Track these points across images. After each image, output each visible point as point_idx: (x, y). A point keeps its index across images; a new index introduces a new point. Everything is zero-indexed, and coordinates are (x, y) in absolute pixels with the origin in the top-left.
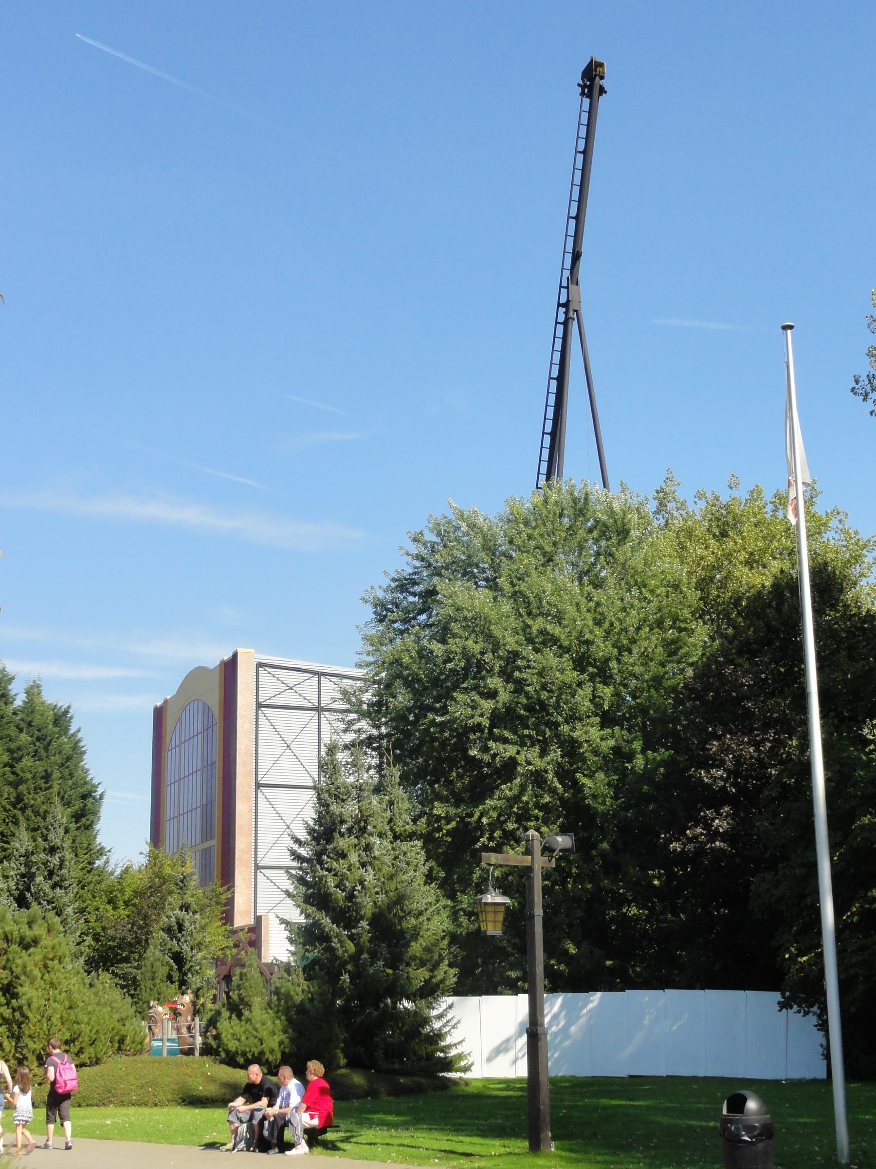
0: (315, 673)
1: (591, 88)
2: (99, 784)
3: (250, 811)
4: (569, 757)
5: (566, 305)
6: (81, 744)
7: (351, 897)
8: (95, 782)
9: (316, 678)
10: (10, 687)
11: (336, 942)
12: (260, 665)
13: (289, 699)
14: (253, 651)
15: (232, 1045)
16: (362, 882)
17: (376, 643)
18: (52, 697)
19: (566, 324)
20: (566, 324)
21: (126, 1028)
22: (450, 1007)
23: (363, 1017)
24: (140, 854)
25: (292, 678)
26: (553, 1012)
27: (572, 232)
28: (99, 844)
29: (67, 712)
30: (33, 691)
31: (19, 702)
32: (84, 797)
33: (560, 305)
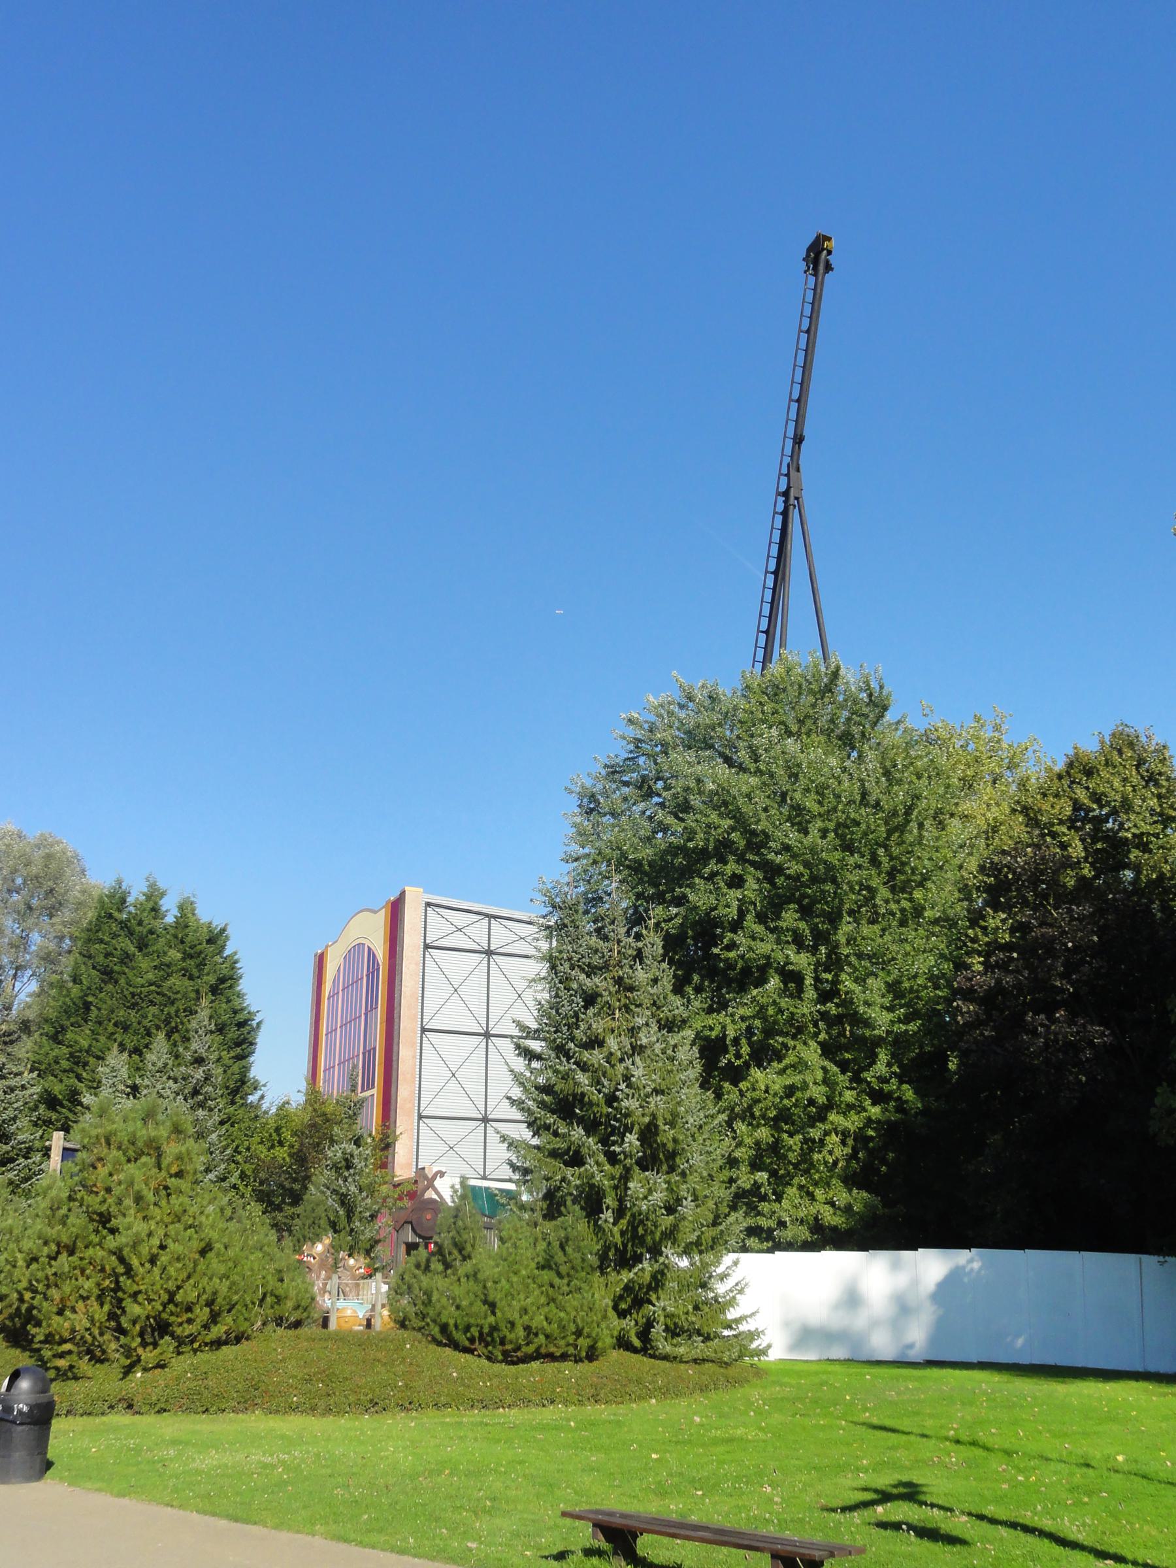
1: (816, 262)
2: (258, 1012)
3: (414, 1057)
4: (323, 1269)
5: (786, 494)
6: (238, 965)
7: (611, 1099)
10: (161, 902)
11: (592, 1163)
12: (428, 905)
13: (458, 941)
14: (422, 890)
15: (450, 1315)
16: (627, 1078)
17: (583, 836)
18: (208, 914)
19: (785, 514)
20: (785, 514)
22: (736, 1263)
23: (631, 1275)
24: (299, 1091)
25: (460, 919)
27: (793, 416)
28: (254, 1078)
29: (223, 930)
30: (186, 908)
31: (170, 919)
32: (241, 1025)
33: (778, 494)
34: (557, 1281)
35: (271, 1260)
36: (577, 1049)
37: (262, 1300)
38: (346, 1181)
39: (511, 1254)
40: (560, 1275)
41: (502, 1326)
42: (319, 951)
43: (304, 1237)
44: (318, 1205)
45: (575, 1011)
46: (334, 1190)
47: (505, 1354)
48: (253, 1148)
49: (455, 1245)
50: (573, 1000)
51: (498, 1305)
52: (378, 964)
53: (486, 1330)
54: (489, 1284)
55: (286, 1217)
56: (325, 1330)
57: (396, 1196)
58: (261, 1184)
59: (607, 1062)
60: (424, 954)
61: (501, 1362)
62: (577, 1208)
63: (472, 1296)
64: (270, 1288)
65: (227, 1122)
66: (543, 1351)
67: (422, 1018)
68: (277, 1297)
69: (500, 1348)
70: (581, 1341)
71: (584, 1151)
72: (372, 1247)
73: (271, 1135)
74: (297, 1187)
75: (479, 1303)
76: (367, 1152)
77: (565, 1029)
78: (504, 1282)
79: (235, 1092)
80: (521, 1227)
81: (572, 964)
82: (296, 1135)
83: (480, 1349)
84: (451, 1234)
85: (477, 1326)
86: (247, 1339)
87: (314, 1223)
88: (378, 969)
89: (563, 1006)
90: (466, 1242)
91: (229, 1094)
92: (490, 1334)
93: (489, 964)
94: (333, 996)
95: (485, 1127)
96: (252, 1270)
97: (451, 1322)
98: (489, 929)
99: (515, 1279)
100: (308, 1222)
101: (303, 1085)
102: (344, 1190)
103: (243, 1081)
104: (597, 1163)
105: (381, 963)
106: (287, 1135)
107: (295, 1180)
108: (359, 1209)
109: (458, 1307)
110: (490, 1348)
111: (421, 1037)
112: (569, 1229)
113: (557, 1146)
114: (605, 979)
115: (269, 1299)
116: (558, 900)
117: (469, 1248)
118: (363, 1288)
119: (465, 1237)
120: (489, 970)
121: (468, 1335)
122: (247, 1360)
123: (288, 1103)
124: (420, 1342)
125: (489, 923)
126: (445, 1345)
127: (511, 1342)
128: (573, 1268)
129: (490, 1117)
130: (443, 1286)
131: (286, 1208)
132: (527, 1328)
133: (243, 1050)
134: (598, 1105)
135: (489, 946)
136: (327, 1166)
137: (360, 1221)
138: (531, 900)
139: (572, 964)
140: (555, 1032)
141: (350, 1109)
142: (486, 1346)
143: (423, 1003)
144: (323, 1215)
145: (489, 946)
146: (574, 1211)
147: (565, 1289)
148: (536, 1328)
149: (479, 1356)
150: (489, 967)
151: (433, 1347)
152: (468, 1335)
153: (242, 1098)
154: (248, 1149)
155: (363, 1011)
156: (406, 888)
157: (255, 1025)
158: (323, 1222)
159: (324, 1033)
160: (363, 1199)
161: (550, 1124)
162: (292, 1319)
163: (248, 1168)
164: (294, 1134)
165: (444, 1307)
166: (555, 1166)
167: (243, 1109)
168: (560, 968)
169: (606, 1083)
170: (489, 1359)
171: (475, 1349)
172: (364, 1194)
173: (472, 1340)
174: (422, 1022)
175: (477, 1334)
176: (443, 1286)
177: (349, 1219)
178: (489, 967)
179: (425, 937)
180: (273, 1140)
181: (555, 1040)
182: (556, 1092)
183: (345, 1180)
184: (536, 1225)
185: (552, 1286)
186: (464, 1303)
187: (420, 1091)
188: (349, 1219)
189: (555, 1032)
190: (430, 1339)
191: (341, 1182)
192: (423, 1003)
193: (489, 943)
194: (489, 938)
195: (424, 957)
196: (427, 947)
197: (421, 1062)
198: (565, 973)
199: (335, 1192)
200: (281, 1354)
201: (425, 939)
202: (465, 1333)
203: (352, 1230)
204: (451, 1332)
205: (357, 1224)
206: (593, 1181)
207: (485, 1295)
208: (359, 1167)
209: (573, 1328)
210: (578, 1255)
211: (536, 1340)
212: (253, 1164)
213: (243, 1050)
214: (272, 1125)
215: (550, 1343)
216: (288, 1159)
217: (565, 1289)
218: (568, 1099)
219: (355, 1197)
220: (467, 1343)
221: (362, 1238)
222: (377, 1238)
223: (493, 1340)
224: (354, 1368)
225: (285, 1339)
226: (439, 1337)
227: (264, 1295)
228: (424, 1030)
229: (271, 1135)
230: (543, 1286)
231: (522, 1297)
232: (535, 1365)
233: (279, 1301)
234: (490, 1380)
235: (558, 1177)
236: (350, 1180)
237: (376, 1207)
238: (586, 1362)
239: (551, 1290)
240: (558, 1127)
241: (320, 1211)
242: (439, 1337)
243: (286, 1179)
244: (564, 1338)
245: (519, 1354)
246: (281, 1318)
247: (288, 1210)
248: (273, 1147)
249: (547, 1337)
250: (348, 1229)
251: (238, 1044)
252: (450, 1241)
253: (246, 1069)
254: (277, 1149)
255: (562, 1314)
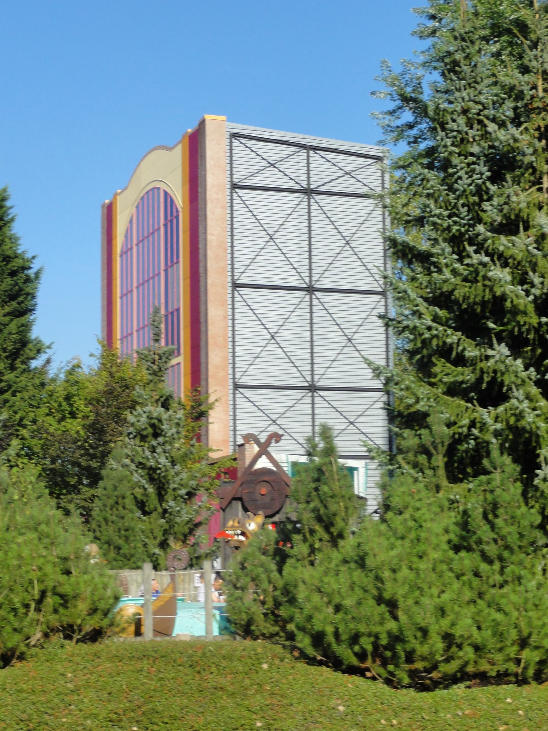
0: (303, 146)
2: (33, 258)
3: (225, 317)
8: (28, 255)
9: (304, 153)
11: (522, 398)
12: (234, 136)
14: (224, 118)
21: (73, 579)
24: (91, 355)
26: (457, 378)
28: (35, 339)
34: (484, 567)
35: (52, 544)
36: (489, 234)
37: (40, 602)
38: (154, 451)
39: (410, 529)
40: (486, 558)
41: (409, 634)
42: (107, 201)
43: (106, 520)
44: (121, 481)
45: (477, 185)
46: (140, 463)
47: (413, 674)
48: (40, 420)
49: (319, 519)
50: (473, 171)
51: (401, 604)
52: (177, 211)
53: (384, 641)
54: (386, 574)
55: (85, 500)
56: (139, 639)
57: (214, 475)
58: (53, 462)
59: (538, 249)
60: (232, 196)
61: (409, 686)
62: (507, 459)
63: (359, 592)
64: (50, 584)
65: (6, 391)
66: (470, 669)
67: (233, 272)
68: (62, 596)
69: (407, 667)
70: (526, 654)
71: (508, 379)
72: (191, 531)
73: (60, 405)
74: (94, 464)
75: (372, 602)
76: (178, 416)
77: (464, 211)
78: (405, 572)
79: (14, 355)
80: (419, 491)
81: (469, 119)
82: (91, 404)
83: (376, 669)
84: (312, 505)
85: (370, 635)
86: (22, 657)
87: (117, 503)
88: (177, 217)
89: (460, 178)
90: (335, 515)
91: (7, 357)
92: (390, 647)
93: (309, 205)
94: (126, 252)
95: (313, 397)
96: (20, 557)
97: (329, 630)
98: (308, 163)
99: (422, 565)
100: (111, 501)
101: (97, 349)
102: (152, 463)
103: (24, 343)
104: (528, 397)
105: (180, 209)
106: (80, 404)
107: (93, 457)
108: (172, 486)
109: (338, 608)
110: (391, 667)
111: (233, 294)
112: (498, 492)
113: (460, 378)
114: (526, 129)
115: (50, 601)
116: (409, 89)
117: (340, 524)
118: (183, 581)
119: (333, 507)
120: (309, 213)
121: (357, 648)
122: (21, 691)
123: (79, 367)
124: (282, 660)
125: (308, 156)
126: (320, 663)
127: (424, 659)
128: (507, 547)
129: (319, 385)
130: (312, 577)
131: (85, 489)
132: (448, 638)
133: (19, 303)
134: (525, 313)
135: (309, 184)
136: (130, 433)
137: (175, 499)
138: (373, 93)
139: (469, 119)
140: (450, 216)
141: (153, 363)
142: (384, 664)
143: (232, 254)
144: (128, 493)
145: (309, 184)
146: (503, 465)
147: (498, 578)
148: (462, 636)
149: (374, 678)
150: (309, 209)
151: (301, 666)
152: (357, 648)
153: (23, 363)
154: (34, 421)
155: (162, 267)
156: (207, 117)
157: (32, 276)
158: (129, 502)
159: (119, 337)
160: (177, 474)
161: (451, 345)
162: (88, 628)
163: (36, 444)
164: (89, 402)
165: (316, 609)
166: (459, 406)
167: (25, 375)
168: (451, 125)
169: (537, 280)
170: (388, 682)
171: (368, 670)
172: (178, 467)
173: (362, 656)
174: (233, 276)
175: (369, 648)
176: (312, 577)
177: (161, 497)
178: (309, 209)
179: (231, 174)
180: (63, 411)
181: (449, 228)
182: (456, 302)
183: (153, 450)
184: (438, 488)
185: (477, 574)
186: (348, 602)
187: (234, 356)
188: (161, 497)
189: (450, 216)
190: (296, 654)
191: (148, 453)
192: (232, 254)
193: (309, 181)
194: (308, 174)
195: (232, 199)
196: (235, 186)
197: (233, 323)
198: (459, 132)
199: (140, 465)
200: (71, 681)
201: (232, 178)
202: (351, 646)
203: (165, 511)
204: (329, 645)
205: (172, 503)
206: (523, 423)
207: (378, 589)
208: (169, 434)
209: (513, 634)
210: (513, 529)
211: (461, 654)
212: (40, 439)
213: (19, 303)
214: (61, 393)
215: (480, 657)
216: (82, 433)
217: (498, 578)
218: (475, 310)
219: (167, 471)
220: (355, 661)
221: (178, 520)
222: (197, 520)
223: (395, 656)
224: (185, 702)
225: (77, 659)
226: (311, 651)
227: (43, 593)
228: (236, 286)
229: (60, 405)
230: (463, 574)
231: (435, 591)
232: (459, 690)
233: (66, 601)
234: (396, 715)
235: (466, 422)
236: (159, 450)
237: (193, 483)
238: (534, 684)
239: (476, 582)
240: (464, 349)
241: (124, 489)
242: (311, 651)
243: (82, 455)
244: (501, 650)
245: (434, 675)
246: (71, 626)
247: (86, 492)
248: (63, 419)
249: (477, 648)
250: (160, 510)
251: (13, 297)
252: (312, 515)
253: (25, 328)
254: (69, 421)
255: (499, 616)
